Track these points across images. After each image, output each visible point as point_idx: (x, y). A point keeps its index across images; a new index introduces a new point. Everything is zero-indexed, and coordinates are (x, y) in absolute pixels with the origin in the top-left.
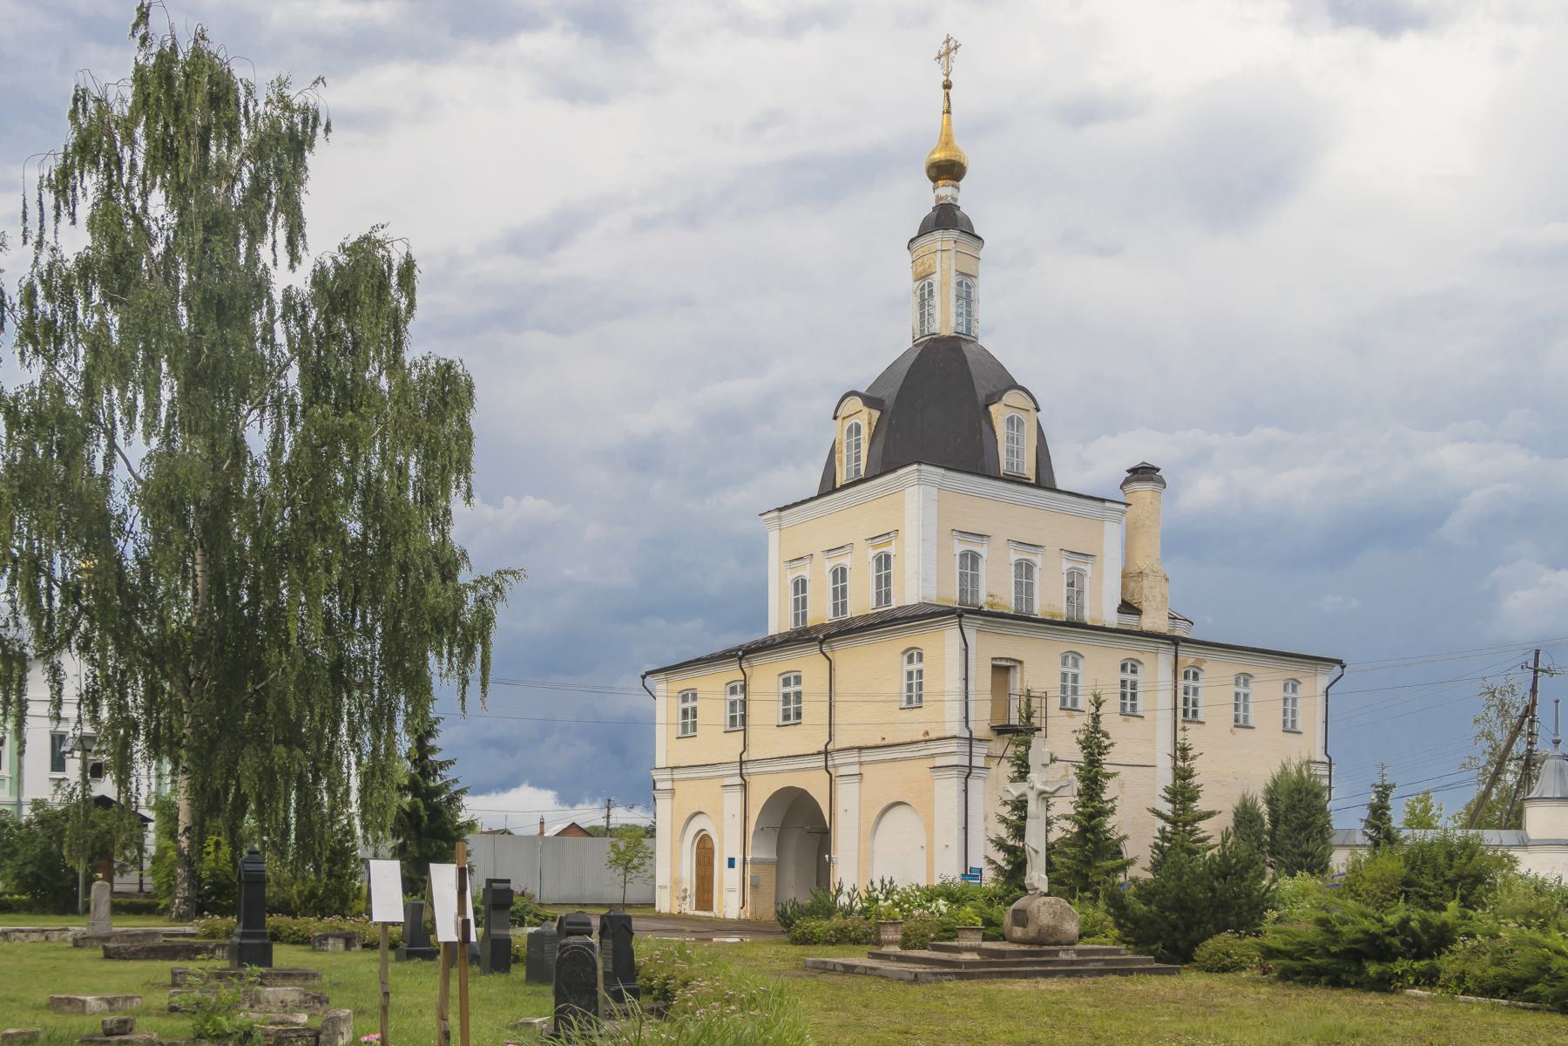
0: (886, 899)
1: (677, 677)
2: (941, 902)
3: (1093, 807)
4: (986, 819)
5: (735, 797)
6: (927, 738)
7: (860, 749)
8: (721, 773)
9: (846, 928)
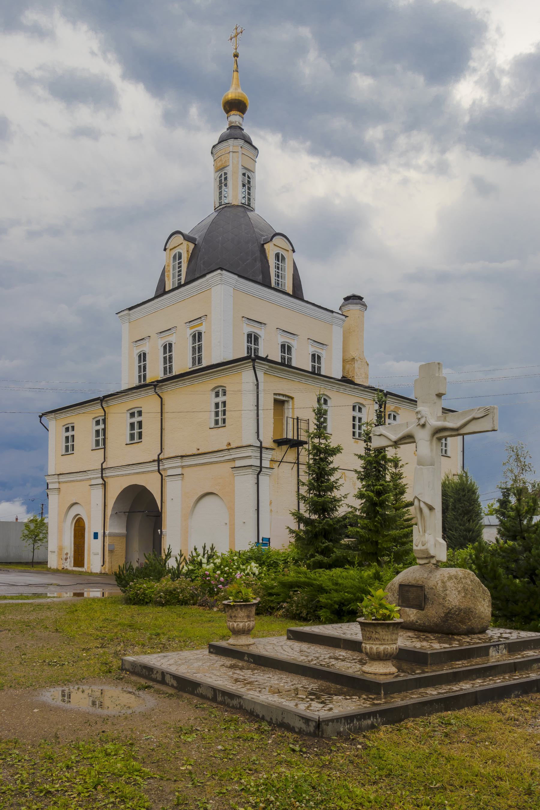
0: (208, 562)
1: (63, 416)
2: (253, 564)
3: (381, 485)
4: (271, 503)
5: (99, 491)
6: (230, 447)
7: (182, 457)
8: (90, 477)
9: (174, 590)
